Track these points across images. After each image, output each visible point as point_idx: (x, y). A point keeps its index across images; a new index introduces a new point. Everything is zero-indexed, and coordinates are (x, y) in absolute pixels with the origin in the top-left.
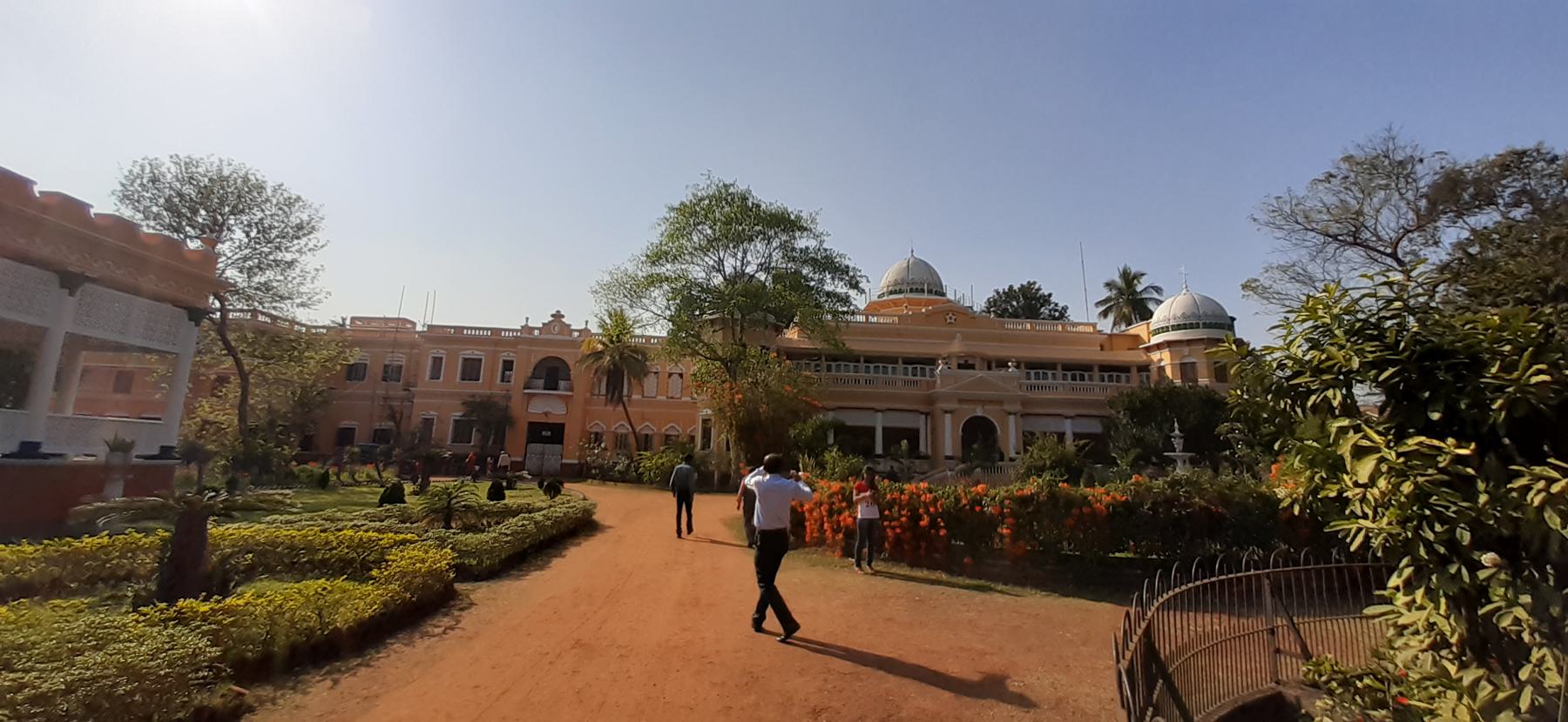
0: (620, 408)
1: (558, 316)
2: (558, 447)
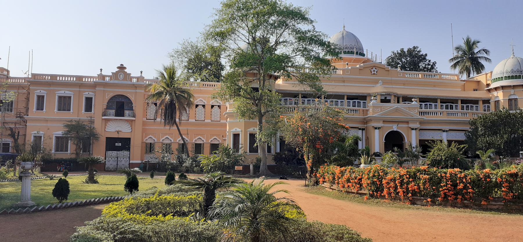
0: (175, 127)
1: (122, 68)
2: (126, 153)
